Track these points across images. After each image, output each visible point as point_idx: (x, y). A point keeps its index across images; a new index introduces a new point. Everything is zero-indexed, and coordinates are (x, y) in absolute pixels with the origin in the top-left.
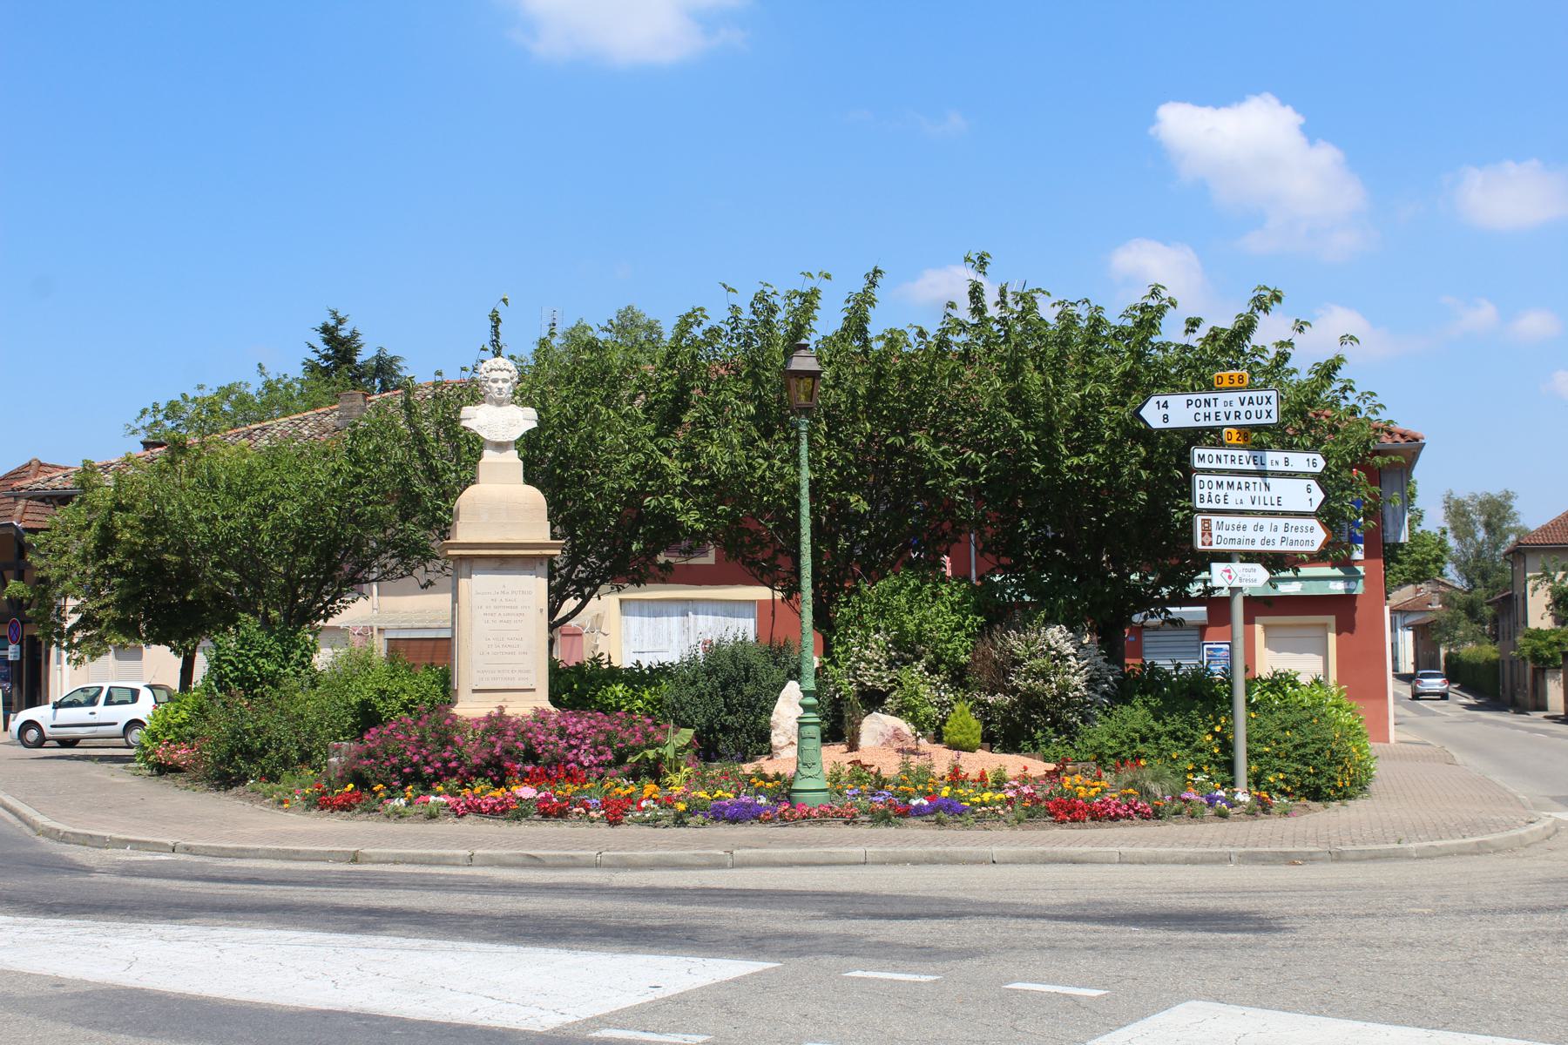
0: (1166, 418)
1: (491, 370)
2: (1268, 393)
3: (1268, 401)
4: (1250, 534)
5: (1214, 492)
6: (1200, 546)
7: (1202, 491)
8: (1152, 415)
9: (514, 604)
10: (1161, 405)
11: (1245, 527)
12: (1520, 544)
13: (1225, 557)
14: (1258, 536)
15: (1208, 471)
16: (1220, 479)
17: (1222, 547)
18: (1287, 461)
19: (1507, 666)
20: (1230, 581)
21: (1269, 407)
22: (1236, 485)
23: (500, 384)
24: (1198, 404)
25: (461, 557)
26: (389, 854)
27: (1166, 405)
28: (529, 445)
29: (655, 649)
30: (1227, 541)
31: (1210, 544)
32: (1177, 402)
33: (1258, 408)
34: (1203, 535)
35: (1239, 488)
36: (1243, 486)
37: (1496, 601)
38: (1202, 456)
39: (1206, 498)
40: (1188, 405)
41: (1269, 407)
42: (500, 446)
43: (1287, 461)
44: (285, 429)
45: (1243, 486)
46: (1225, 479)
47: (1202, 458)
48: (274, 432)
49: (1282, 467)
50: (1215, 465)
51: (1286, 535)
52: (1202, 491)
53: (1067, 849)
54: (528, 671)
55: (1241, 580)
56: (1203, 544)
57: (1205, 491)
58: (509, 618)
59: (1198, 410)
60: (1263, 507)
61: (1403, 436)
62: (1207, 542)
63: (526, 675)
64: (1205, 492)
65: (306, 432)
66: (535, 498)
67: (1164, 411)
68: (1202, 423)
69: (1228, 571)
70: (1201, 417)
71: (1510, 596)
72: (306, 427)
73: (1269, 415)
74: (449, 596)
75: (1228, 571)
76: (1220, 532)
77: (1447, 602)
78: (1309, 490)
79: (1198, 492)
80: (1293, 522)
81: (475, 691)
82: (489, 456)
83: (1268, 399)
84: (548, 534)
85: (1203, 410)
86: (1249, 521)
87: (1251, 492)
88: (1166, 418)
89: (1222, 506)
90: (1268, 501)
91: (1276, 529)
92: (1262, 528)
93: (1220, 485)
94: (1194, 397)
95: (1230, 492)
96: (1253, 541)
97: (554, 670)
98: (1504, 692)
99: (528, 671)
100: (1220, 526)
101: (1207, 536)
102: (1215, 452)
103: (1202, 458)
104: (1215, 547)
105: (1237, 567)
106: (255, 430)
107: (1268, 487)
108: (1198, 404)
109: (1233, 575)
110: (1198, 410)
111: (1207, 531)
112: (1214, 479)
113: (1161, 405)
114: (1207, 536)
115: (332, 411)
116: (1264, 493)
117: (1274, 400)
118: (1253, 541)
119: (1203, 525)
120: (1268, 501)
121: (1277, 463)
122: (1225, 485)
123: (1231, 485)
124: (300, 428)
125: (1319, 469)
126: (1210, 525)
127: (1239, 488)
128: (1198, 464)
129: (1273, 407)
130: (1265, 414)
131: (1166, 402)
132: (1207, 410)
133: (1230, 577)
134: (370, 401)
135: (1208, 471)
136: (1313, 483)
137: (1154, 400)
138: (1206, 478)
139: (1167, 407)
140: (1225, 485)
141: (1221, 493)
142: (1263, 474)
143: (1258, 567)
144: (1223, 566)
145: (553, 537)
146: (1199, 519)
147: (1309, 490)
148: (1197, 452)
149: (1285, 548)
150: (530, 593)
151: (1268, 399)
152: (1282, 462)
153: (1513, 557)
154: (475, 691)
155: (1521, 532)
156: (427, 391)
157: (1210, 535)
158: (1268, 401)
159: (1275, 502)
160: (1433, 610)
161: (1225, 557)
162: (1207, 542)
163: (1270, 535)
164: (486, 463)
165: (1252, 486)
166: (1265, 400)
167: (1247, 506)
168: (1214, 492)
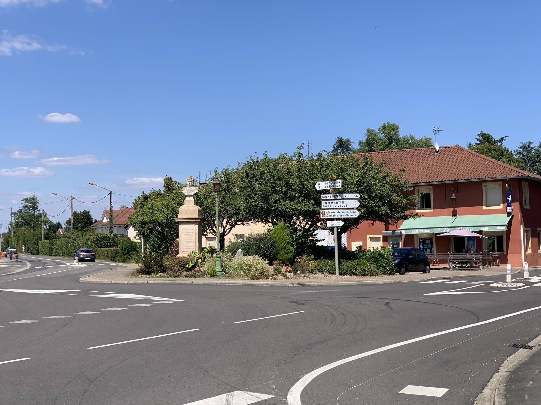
0: (320, 187)
4: (336, 214)
6: (322, 217)
7: (324, 205)
8: (317, 187)
9: (190, 232)
14: (339, 214)
15: (324, 200)
16: (329, 201)
18: (348, 196)
20: (332, 225)
21: (339, 184)
22: (334, 203)
26: (278, 284)
28: (196, 196)
31: (325, 217)
32: (322, 183)
36: (336, 203)
38: (323, 196)
39: (325, 206)
41: (339, 184)
42: (189, 196)
43: (348, 196)
45: (336, 203)
46: (330, 201)
47: (323, 197)
49: (347, 197)
50: (327, 198)
51: (347, 214)
52: (324, 205)
54: (194, 247)
55: (335, 225)
56: (323, 217)
57: (324, 204)
59: (326, 185)
60: (341, 207)
63: (193, 248)
64: (325, 205)
68: (327, 188)
69: (332, 223)
70: (326, 187)
74: (415, 187)
78: (355, 202)
80: (349, 210)
81: (182, 251)
85: (327, 185)
86: (336, 211)
87: (338, 204)
88: (320, 187)
89: (330, 208)
90: (345, 206)
92: (340, 212)
93: (329, 203)
94: (325, 182)
95: (332, 204)
96: (337, 216)
99: (194, 247)
102: (327, 195)
103: (323, 197)
104: (326, 217)
107: (343, 202)
109: (333, 224)
110: (326, 185)
112: (327, 201)
117: (340, 182)
118: (337, 216)
121: (346, 197)
122: (330, 203)
123: (332, 203)
127: (335, 203)
129: (340, 184)
135: (324, 200)
136: (357, 201)
137: (317, 183)
138: (325, 201)
140: (330, 203)
141: (329, 205)
142: (343, 199)
143: (341, 221)
147: (355, 202)
148: (322, 195)
149: (347, 217)
150: (194, 229)
154: (182, 251)
157: (325, 215)
159: (345, 206)
164: (186, 201)
165: (338, 202)
167: (337, 207)
168: (327, 204)
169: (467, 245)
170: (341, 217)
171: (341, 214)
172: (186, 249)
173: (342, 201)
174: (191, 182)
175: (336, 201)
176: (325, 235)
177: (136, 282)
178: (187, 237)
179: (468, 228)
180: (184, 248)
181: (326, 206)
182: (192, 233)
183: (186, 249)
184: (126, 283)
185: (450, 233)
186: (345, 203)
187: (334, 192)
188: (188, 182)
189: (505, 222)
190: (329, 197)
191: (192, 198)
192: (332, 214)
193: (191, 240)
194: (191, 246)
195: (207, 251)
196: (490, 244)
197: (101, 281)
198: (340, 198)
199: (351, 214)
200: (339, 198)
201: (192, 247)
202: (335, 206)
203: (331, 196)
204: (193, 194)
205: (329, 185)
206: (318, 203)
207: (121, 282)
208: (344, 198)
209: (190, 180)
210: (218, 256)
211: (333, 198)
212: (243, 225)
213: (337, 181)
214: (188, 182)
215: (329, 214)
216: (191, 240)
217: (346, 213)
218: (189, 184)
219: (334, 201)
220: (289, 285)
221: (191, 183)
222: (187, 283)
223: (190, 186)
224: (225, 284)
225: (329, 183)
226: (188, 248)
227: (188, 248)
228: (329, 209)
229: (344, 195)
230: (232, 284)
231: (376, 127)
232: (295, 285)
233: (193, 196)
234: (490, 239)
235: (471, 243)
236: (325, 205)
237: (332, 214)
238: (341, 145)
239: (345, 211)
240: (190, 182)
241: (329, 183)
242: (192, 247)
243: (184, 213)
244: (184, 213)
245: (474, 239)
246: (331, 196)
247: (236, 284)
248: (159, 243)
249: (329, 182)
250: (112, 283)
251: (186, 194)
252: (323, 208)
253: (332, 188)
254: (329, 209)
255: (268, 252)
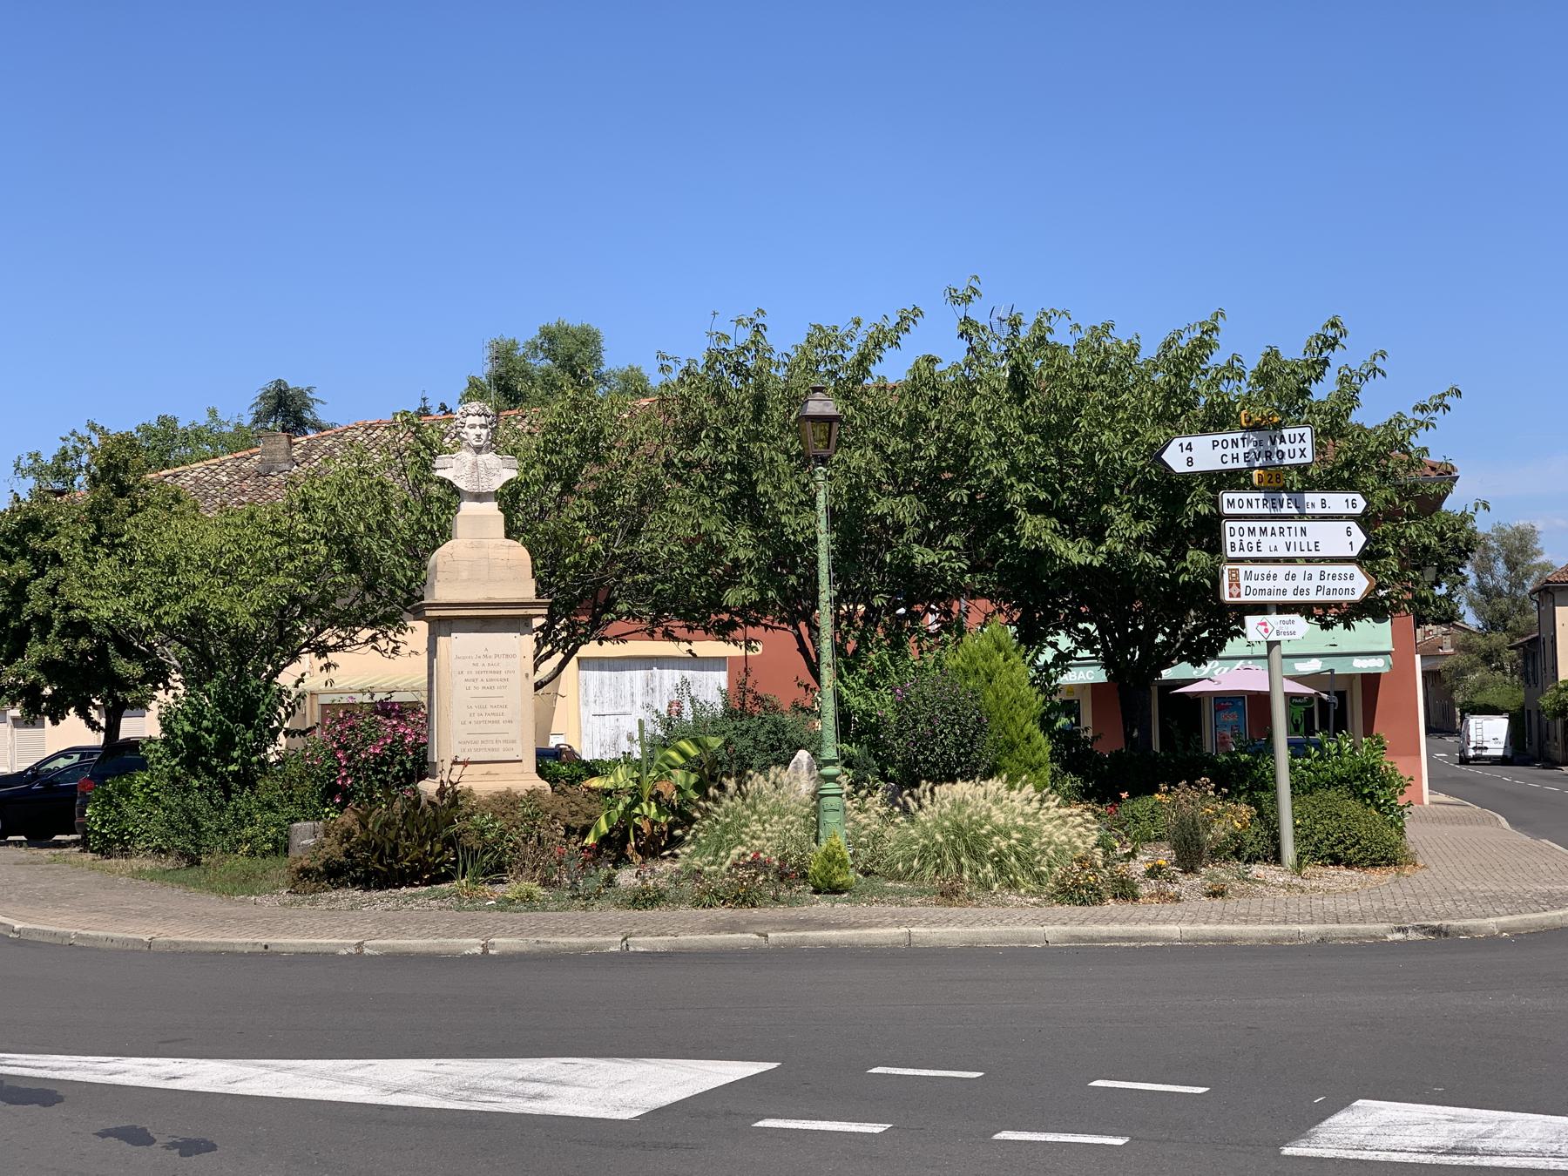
0: (1190, 461)
1: (468, 415)
2: (1301, 431)
3: (1302, 439)
4: (1280, 583)
5: (1246, 539)
6: (1227, 598)
7: (1232, 539)
8: (1175, 458)
10: (1184, 447)
11: (1275, 576)
12: (1548, 582)
13: (1261, 609)
14: (1290, 586)
16: (1252, 524)
17: (1251, 598)
19: (1534, 718)
20: (1266, 635)
21: (1302, 445)
23: (478, 430)
24: (1225, 445)
25: (440, 619)
27: (1189, 448)
28: (509, 498)
29: (617, 711)
30: (1255, 592)
31: (1239, 596)
32: (1202, 443)
33: (1291, 447)
34: (1231, 586)
35: (1273, 534)
37: (1520, 645)
39: (1237, 547)
40: (1214, 446)
41: (1302, 445)
42: (479, 497)
44: (202, 475)
46: (1257, 525)
47: (1231, 503)
48: (188, 478)
49: (1318, 510)
51: (1322, 583)
52: (1232, 539)
53: (1025, 929)
54: (514, 742)
55: (1278, 633)
56: (1231, 596)
57: (1234, 537)
58: (491, 684)
59: (1225, 452)
61: (1433, 469)
62: (1235, 594)
64: (1236, 540)
65: (225, 479)
66: (518, 553)
67: (1187, 454)
68: (1230, 466)
69: (1264, 624)
70: (1229, 459)
71: (1537, 639)
72: (224, 473)
73: (1303, 454)
75: (1264, 624)
76: (1248, 583)
77: (1466, 648)
78: (1349, 533)
79: (1229, 539)
82: (467, 507)
83: (1302, 437)
84: (534, 593)
85: (1230, 451)
86: (1281, 570)
87: (1287, 538)
88: (1190, 461)
89: (1255, 554)
90: (1305, 547)
91: (1310, 578)
92: (1294, 576)
93: (1252, 532)
94: (1220, 438)
95: (1263, 539)
96: (1285, 592)
97: (22, 722)
98: (1530, 744)
99: (514, 742)
100: (1248, 576)
101: (1234, 587)
102: (1245, 496)
103: (1231, 503)
104: (1244, 598)
105: (1273, 619)
106: (166, 477)
107: (1303, 531)
108: (1225, 445)
109: (1270, 629)
110: (1225, 452)
111: (1235, 582)
112: (1246, 525)
113: (1184, 447)
114: (1234, 587)
115: (253, 455)
116: (1299, 539)
117: (1308, 437)
118: (1285, 592)
119: (1230, 575)
120: (1305, 547)
121: (1313, 505)
122: (1258, 531)
123: (1263, 531)
124: (217, 474)
125: (1359, 510)
126: (1238, 575)
127: (1273, 534)
128: (1227, 510)
129: (1308, 445)
130: (1298, 453)
131: (1190, 444)
132: (1235, 451)
133: (1266, 631)
134: (295, 444)
136: (1353, 525)
137: (1176, 442)
138: (1236, 525)
139: (1191, 449)
140: (1258, 531)
141: (1254, 539)
142: (1302, 516)
144: (1259, 618)
145: (538, 596)
146: (1226, 568)
147: (1349, 533)
148: (1226, 497)
151: (1302, 437)
152: (1318, 504)
153: (1540, 596)
155: (1545, 567)
156: (358, 433)
157: (1238, 586)
158: (1302, 439)
159: (1312, 547)
160: (1446, 655)
161: (1261, 609)
162: (1235, 594)
163: (1304, 585)
165: (1287, 531)
166: (1298, 438)
168: (1246, 539)
169: (1216, 726)
170: (1299, 598)
171: (1300, 583)
172: (476, 750)
173: (1299, 525)
174: (486, 427)
175: (1277, 525)
176: (635, 691)
177: (545, 946)
178: (481, 692)
179: (1241, 662)
180: (468, 746)
181: (1242, 549)
182: (504, 676)
183: (476, 750)
184: (478, 950)
185: (1219, 683)
186: (1311, 538)
187: (1269, 482)
188: (473, 426)
189: (1381, 643)
190: (1250, 503)
191: (492, 508)
192: (1266, 585)
193: (500, 710)
194: (501, 737)
195: (681, 761)
196: (1297, 721)
197: (265, 941)
198: (1294, 511)
199: (1338, 584)
200: (1285, 510)
201: (505, 741)
202: (1276, 550)
203: (1253, 502)
204: (496, 484)
205: (1241, 450)
206: (1209, 531)
207: (437, 949)
208: (1307, 511)
209: (483, 420)
210: (831, 785)
211: (1266, 511)
212: (601, 644)
213: (1286, 432)
214: (473, 426)
215: (1253, 584)
216: (500, 710)
217: (1316, 581)
218: (479, 436)
219: (1269, 525)
220: (1390, 937)
221: (484, 432)
222: (880, 940)
223: (478, 450)
224: (1093, 940)
225: (1240, 442)
226: (483, 746)
227: (483, 746)
228: (1256, 561)
229: (1309, 497)
230: (1130, 939)
231: (524, 332)
232: (1412, 936)
233: (497, 496)
234: (1295, 704)
235: (1230, 717)
236: (1236, 540)
237: (1266, 585)
238: (279, 405)
239: (1315, 570)
240: (482, 426)
241: (1240, 442)
242: (505, 741)
243: (465, 575)
244: (465, 575)
245: (1240, 703)
246: (1257, 500)
247: (1149, 939)
248: (228, 726)
249: (1240, 436)
250: (367, 951)
251: (461, 484)
252: (1230, 554)
253: (1257, 464)
254: (1256, 561)
255: (966, 762)
